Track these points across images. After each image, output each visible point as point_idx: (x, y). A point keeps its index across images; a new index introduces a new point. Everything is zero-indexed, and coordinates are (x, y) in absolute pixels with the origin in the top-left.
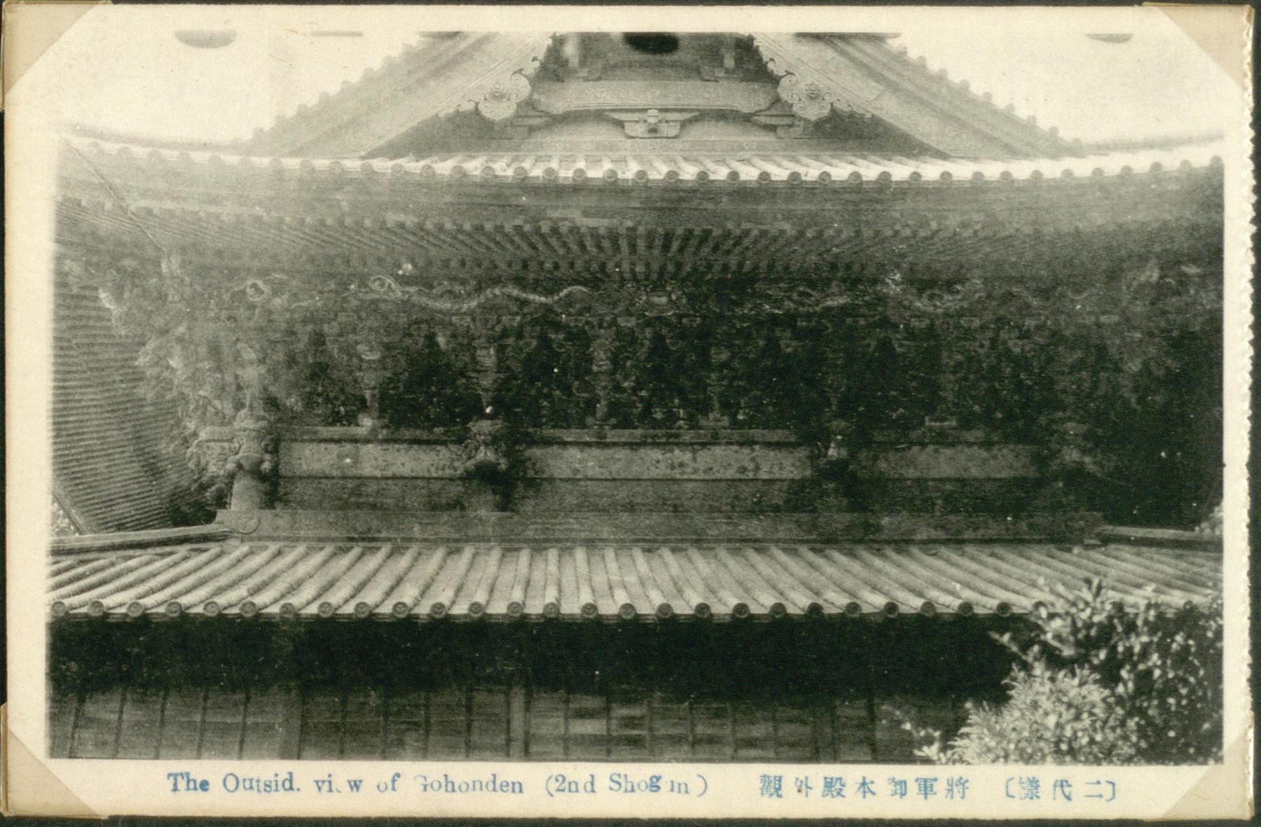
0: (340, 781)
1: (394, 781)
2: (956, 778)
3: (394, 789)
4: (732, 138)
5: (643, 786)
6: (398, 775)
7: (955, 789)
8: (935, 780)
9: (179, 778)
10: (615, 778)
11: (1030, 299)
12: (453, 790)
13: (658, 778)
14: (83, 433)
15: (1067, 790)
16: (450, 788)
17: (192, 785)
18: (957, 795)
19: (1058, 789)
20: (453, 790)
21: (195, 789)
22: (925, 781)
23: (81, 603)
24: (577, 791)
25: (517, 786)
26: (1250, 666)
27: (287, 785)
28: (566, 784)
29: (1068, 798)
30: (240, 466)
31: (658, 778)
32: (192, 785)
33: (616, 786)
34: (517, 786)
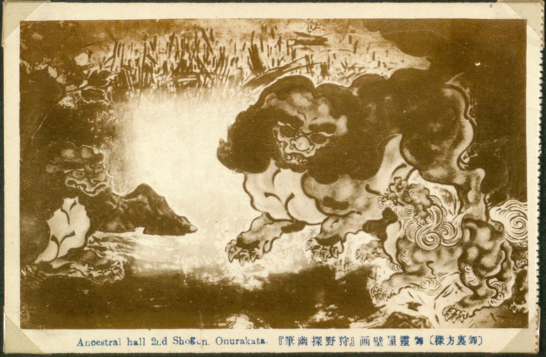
5: (188, 342)
10: (176, 338)
13: (194, 338)
17: (130, 343)
28: (156, 342)
31: (194, 338)
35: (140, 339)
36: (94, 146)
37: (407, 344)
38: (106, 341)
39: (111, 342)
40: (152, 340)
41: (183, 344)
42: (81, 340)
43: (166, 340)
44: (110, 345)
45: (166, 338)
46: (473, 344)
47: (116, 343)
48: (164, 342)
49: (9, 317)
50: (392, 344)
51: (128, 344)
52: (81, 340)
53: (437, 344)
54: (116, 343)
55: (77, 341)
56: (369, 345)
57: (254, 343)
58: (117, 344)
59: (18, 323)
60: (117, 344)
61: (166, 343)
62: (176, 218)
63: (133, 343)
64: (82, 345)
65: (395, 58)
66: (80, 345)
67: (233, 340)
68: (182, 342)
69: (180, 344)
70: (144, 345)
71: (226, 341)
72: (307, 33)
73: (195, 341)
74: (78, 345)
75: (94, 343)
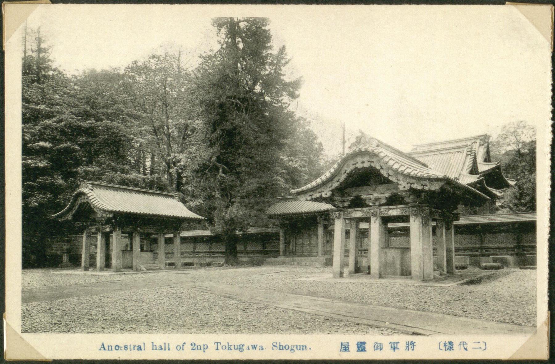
0: (387, 347)
1: (183, 346)
3: (183, 350)
7: (410, 347)
8: (398, 343)
9: (219, 344)
10: (275, 344)
16: (155, 348)
17: (154, 347)
19: (462, 346)
20: (156, 349)
23: (399, 274)
24: (112, 350)
28: (196, 346)
29: (466, 349)
30: (237, 178)
32: (154, 347)
34: (304, 347)
37: (363, 350)
39: (134, 346)
41: (283, 349)
47: (140, 348)
49: (10, 323)
50: (394, 349)
52: (103, 344)
54: (140, 348)
55: (100, 345)
56: (342, 344)
57: (162, 349)
58: (141, 350)
59: (19, 329)
60: (141, 350)
64: (105, 349)
66: (102, 349)
68: (281, 348)
69: (280, 349)
70: (169, 349)
71: (199, 347)
72: (445, 316)
75: (117, 348)
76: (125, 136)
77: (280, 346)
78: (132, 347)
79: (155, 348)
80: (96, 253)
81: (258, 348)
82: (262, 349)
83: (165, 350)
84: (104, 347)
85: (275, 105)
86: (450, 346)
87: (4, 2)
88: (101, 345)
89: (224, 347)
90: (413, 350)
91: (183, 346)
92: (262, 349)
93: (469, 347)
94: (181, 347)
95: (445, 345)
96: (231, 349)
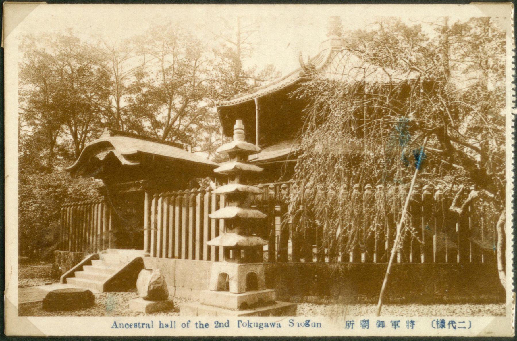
1: (188, 323)
2: (410, 320)
3: (188, 327)
4: (232, 101)
5: (303, 324)
6: (189, 321)
7: (410, 325)
10: (291, 321)
11: (57, 244)
12: (163, 327)
13: (309, 321)
14: (93, 237)
15: (454, 325)
16: (161, 326)
17: (201, 326)
18: (410, 328)
19: (451, 325)
21: (203, 327)
22: (395, 322)
25: (319, 325)
26: (513, 265)
27: (227, 325)
28: (219, 325)
31: (309, 321)
32: (201, 326)
33: (291, 325)
34: (319, 325)
35: (171, 321)
36: (208, 178)
38: (139, 324)
39: (143, 324)
40: (215, 323)
42: (115, 323)
43: (228, 323)
44: (143, 327)
45: (228, 321)
46: (381, 328)
48: (227, 325)
51: (160, 327)
52: (115, 323)
53: (438, 328)
54: (148, 326)
58: (149, 327)
60: (117, 327)
61: (228, 326)
62: (400, 213)
63: (164, 326)
64: (117, 327)
65: (77, 187)
66: (115, 327)
67: (315, 323)
73: (310, 323)
74: (113, 327)
75: (127, 326)
76: (26, 135)
77: (200, 324)
78: (141, 325)
79: (161, 326)
80: (412, 178)
81: (276, 325)
82: (280, 327)
83: (171, 327)
84: (116, 325)
85: (321, 114)
86: (349, 324)
87: (5, 2)
88: (113, 323)
89: (245, 325)
90: (412, 328)
91: (188, 323)
92: (280, 327)
93: (458, 325)
94: (186, 325)
95: (437, 323)
96: (251, 327)
